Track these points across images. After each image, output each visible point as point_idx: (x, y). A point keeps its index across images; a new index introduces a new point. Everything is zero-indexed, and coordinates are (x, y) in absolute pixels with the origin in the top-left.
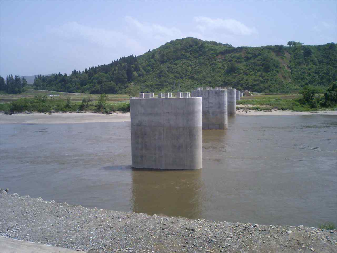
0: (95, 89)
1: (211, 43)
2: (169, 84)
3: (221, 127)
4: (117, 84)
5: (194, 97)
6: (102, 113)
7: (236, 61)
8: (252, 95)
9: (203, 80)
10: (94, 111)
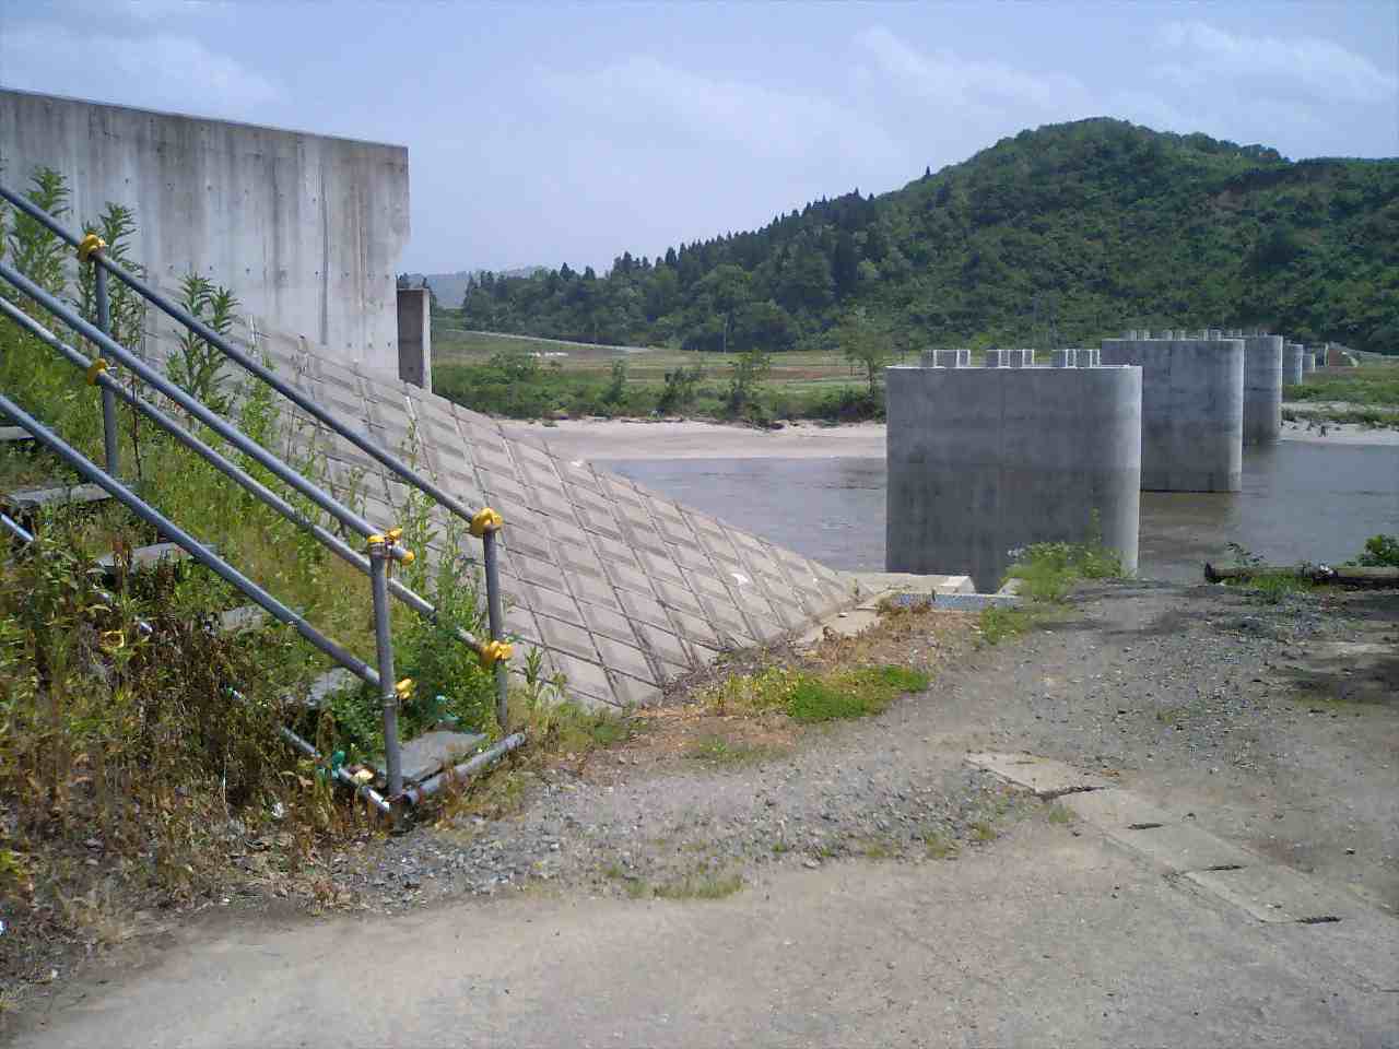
0: (705, 330)
1: (1187, 145)
2: (1008, 310)
3: (1215, 485)
4: (793, 311)
5: (1117, 367)
6: (748, 423)
7: (1293, 219)
8: (1355, 362)
9: (1154, 297)
10: (714, 416)
